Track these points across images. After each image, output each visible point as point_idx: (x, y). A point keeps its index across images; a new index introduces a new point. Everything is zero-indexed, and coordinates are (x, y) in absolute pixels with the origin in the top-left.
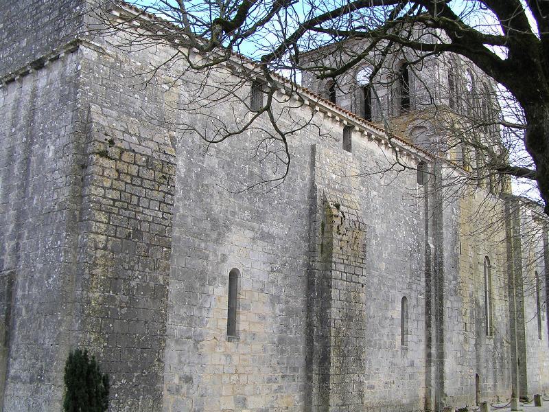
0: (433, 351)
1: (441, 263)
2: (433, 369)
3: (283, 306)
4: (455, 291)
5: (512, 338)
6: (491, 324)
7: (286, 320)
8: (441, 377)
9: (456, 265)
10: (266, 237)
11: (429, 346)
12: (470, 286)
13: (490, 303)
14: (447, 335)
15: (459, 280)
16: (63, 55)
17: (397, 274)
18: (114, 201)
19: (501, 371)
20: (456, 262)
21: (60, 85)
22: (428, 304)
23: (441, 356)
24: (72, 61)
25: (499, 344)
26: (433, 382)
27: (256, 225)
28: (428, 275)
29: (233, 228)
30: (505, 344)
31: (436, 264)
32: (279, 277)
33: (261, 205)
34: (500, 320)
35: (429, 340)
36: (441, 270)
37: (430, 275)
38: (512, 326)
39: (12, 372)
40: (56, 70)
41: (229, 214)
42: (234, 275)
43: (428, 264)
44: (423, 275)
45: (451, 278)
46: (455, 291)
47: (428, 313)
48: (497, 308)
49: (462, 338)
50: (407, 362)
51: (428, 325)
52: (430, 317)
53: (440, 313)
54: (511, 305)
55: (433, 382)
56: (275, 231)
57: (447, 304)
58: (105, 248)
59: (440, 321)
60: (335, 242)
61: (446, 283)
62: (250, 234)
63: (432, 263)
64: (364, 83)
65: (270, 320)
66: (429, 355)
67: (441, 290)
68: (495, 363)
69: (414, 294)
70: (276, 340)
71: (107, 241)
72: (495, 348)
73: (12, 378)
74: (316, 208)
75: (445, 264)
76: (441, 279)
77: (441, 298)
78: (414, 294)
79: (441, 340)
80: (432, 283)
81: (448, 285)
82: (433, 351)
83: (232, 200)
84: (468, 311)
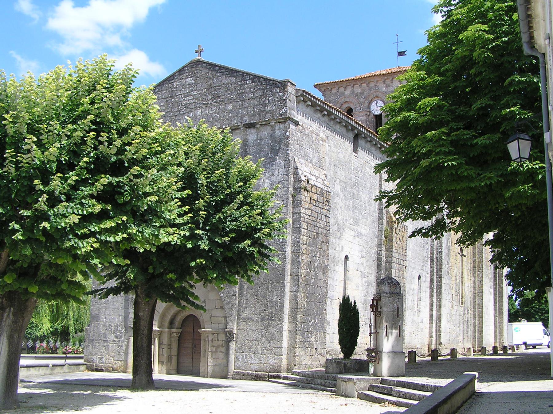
0: (434, 313)
1: (441, 253)
2: (434, 325)
3: (365, 279)
4: (448, 272)
5: (474, 307)
6: (462, 296)
7: (367, 288)
8: (439, 331)
9: (448, 255)
10: (359, 235)
11: (431, 310)
12: (456, 269)
13: (462, 282)
14: (443, 302)
15: (450, 264)
16: (274, 124)
17: (416, 259)
18: (309, 216)
19: (467, 331)
20: (449, 252)
21: (270, 142)
22: (432, 281)
23: (439, 317)
24: (280, 128)
25: (466, 311)
26: (434, 335)
27: (355, 227)
28: (432, 261)
29: (346, 229)
30: (470, 311)
31: (437, 254)
32: (365, 260)
33: (357, 215)
34: (467, 294)
35: (432, 305)
36: (441, 257)
37: (433, 260)
38: (474, 299)
39: (243, 315)
40: (265, 132)
41: (344, 221)
42: (346, 257)
43: (432, 253)
44: (429, 261)
45: (446, 263)
46: (448, 272)
47: (431, 288)
48: (466, 285)
49: (450, 304)
50: (420, 321)
51: (431, 296)
52: (433, 290)
53: (440, 287)
54: (474, 283)
55: (434, 335)
56: (363, 231)
57: (444, 281)
58: (306, 244)
59: (439, 293)
60: (394, 238)
61: (443, 267)
62: (353, 233)
63: (435, 252)
64: (376, 113)
65: (360, 288)
66: (431, 316)
67: (441, 271)
68: (464, 325)
69: (424, 273)
70: (363, 301)
71: (307, 239)
72: (464, 314)
73: (244, 319)
74: (382, 216)
75: (443, 253)
76: (441, 264)
77: (440, 277)
78: (424, 273)
79: (439, 306)
80: (435, 266)
81: (445, 268)
82: (434, 313)
83: (346, 212)
84: (454, 286)
